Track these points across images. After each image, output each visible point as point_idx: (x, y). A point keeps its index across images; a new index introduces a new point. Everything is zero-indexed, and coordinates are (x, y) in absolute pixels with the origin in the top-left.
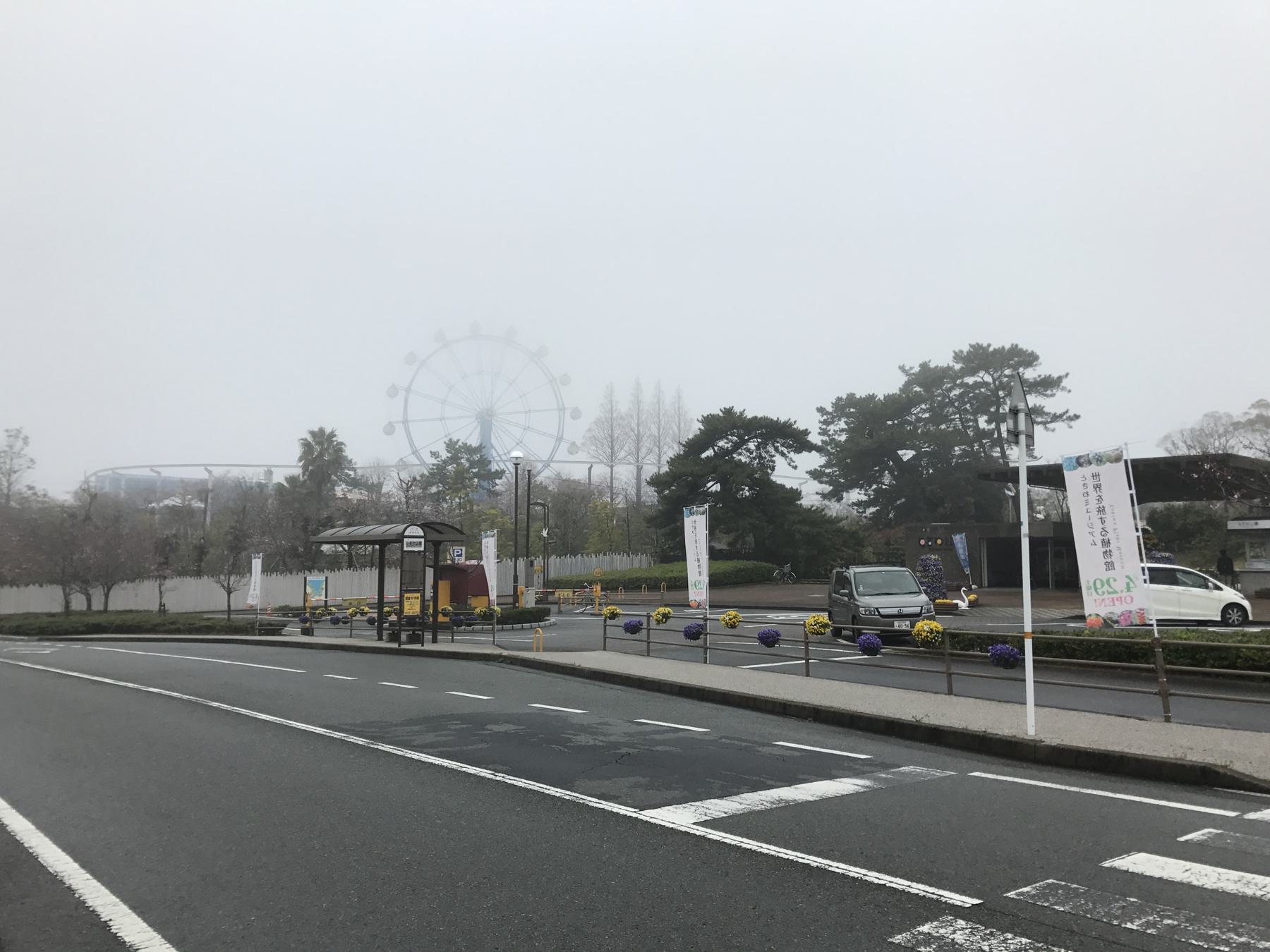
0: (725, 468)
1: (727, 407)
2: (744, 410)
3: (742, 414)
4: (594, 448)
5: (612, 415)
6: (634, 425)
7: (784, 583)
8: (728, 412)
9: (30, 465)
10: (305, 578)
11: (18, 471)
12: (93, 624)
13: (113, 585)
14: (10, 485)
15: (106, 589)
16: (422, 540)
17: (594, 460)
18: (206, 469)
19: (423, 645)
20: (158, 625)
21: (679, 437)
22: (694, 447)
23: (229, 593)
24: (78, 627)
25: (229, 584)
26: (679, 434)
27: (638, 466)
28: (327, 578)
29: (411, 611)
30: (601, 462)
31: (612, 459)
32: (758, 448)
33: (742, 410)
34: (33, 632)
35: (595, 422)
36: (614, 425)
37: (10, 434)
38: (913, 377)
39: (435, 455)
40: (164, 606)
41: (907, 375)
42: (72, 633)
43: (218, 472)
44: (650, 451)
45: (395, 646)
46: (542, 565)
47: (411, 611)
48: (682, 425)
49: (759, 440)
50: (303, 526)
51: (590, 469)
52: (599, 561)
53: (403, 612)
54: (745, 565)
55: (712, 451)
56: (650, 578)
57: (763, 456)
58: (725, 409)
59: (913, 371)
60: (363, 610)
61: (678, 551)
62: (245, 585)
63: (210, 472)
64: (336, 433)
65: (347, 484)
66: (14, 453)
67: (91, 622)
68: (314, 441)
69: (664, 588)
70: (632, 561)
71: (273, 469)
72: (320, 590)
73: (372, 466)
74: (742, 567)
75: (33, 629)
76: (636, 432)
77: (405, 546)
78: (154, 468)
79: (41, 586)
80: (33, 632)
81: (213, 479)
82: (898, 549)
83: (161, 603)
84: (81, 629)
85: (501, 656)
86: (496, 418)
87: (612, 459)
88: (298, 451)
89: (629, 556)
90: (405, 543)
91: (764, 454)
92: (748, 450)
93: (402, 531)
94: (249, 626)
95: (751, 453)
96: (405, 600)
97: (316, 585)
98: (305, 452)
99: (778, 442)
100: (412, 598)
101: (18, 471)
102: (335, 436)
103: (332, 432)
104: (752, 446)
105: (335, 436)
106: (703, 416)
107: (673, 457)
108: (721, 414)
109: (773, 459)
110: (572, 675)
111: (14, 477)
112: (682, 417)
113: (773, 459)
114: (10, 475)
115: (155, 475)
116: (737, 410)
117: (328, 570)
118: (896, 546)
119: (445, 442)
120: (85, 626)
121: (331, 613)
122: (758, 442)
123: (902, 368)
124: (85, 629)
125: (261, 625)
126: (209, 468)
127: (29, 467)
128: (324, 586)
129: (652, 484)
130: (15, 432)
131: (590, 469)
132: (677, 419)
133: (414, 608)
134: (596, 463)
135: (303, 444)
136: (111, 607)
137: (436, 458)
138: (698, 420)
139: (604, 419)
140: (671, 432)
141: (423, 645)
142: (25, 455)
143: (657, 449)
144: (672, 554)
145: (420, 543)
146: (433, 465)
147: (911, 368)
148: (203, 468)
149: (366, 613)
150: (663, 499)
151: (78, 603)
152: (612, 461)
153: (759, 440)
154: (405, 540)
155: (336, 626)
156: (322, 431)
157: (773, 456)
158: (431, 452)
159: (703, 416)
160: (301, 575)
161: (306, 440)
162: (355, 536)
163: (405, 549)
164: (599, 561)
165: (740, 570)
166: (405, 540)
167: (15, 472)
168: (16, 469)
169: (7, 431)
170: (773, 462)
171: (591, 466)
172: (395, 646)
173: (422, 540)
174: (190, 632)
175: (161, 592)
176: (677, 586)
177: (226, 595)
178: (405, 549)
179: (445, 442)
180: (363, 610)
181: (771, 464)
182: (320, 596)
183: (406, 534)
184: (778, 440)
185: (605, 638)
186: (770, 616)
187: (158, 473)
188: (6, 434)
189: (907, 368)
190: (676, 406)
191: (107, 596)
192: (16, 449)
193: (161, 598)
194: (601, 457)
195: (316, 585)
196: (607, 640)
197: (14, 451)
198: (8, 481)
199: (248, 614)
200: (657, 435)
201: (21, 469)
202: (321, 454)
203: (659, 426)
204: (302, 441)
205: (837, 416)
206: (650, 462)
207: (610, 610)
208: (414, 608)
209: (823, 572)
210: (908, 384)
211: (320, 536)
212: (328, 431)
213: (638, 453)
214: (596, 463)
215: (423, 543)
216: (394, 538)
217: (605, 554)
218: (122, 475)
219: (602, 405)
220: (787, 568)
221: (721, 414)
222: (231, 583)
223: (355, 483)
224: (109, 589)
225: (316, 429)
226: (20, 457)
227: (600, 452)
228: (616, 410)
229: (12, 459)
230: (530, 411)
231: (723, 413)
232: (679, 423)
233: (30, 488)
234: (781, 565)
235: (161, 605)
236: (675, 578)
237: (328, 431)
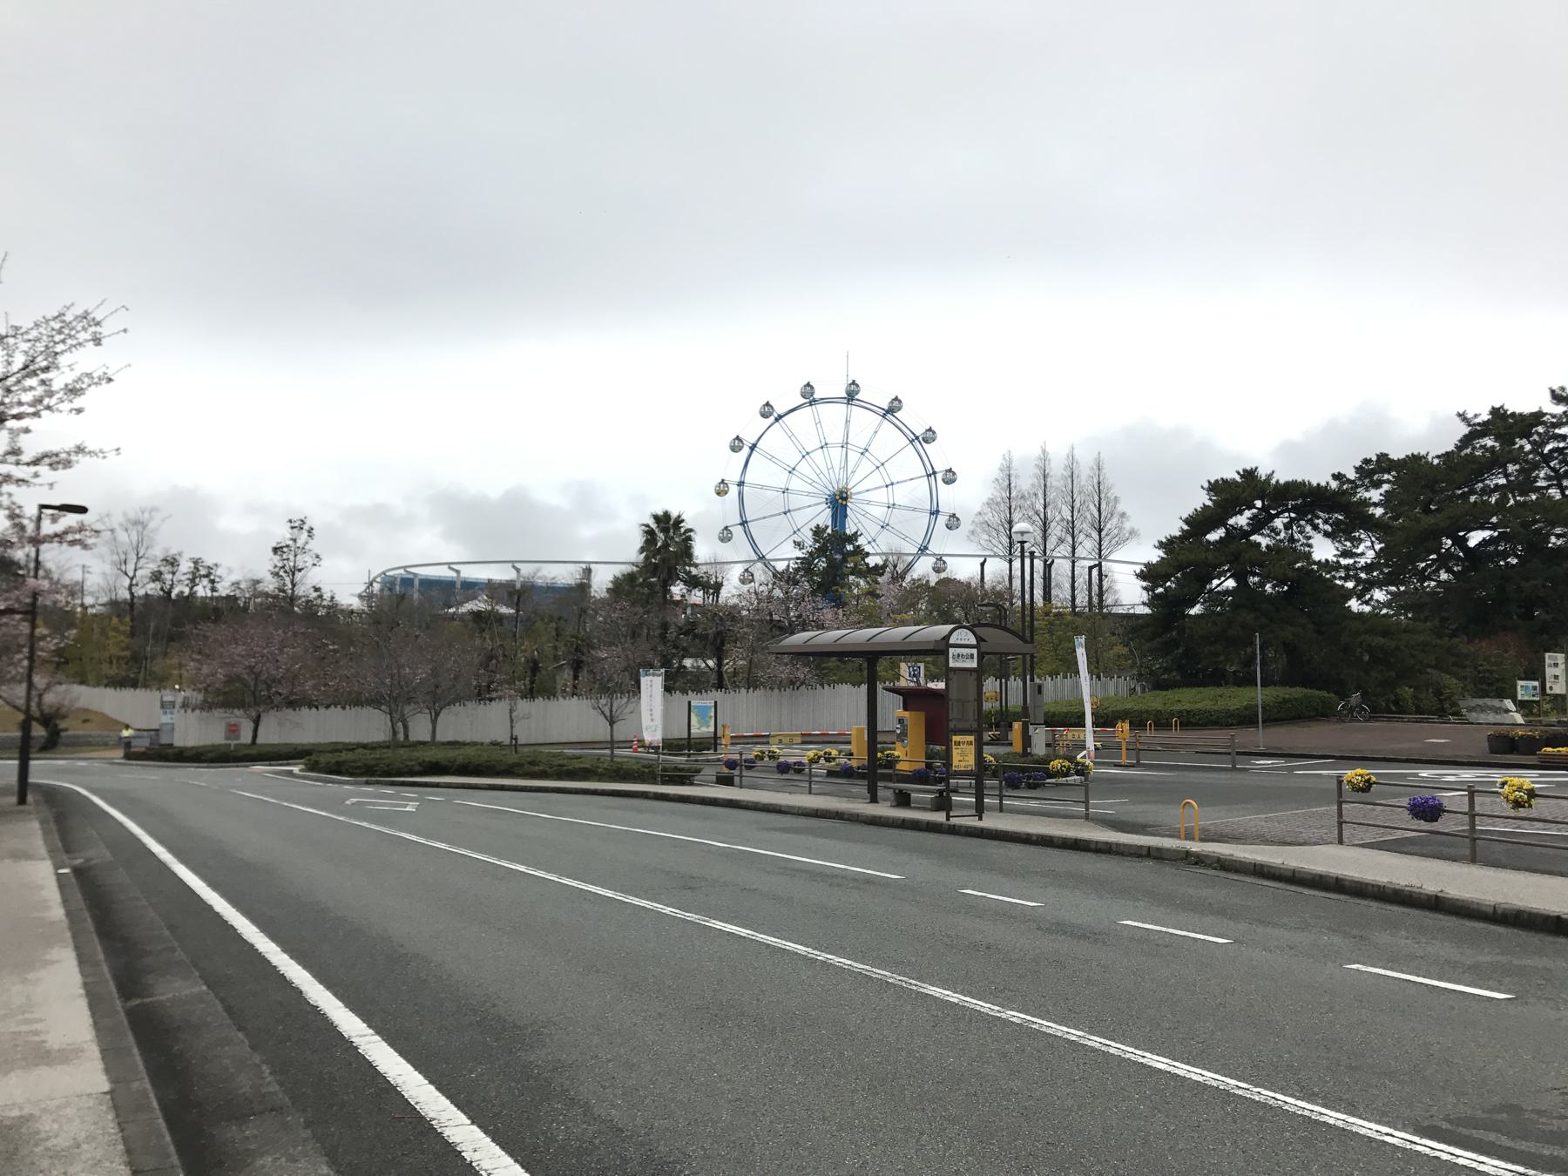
0: (1237, 553)
1: (1248, 468)
2: (1273, 472)
3: (1270, 476)
4: (986, 537)
5: (1010, 494)
6: (1040, 507)
7: (1354, 720)
8: (1249, 475)
9: (315, 562)
10: (689, 703)
11: (302, 569)
12: (430, 762)
13: (441, 709)
14: (294, 585)
15: (433, 714)
16: (975, 651)
17: (988, 553)
18: (514, 567)
19: (980, 819)
20: (516, 765)
21: (1100, 522)
22: (1199, 523)
23: (612, 723)
24: (413, 766)
25: (611, 711)
26: (1100, 518)
27: (1045, 561)
28: (716, 703)
29: (963, 764)
30: (995, 556)
31: (1010, 551)
32: (1287, 526)
33: (1269, 472)
34: (358, 771)
35: (988, 504)
36: (1013, 507)
37: (293, 525)
38: (1479, 428)
39: (799, 545)
40: (516, 739)
41: (1469, 425)
42: (400, 774)
43: (526, 570)
44: (1061, 540)
45: (939, 817)
46: (998, 691)
47: (963, 764)
48: (1103, 506)
49: (1293, 515)
50: (660, 635)
51: (982, 565)
52: (1056, 684)
53: (952, 765)
54: (1291, 694)
55: (1224, 530)
56: (1147, 712)
57: (1296, 537)
58: (1245, 471)
59: (1478, 420)
60: (830, 754)
61: (1174, 674)
62: (631, 712)
63: (518, 570)
64: (683, 517)
65: (686, 583)
66: (299, 548)
67: (427, 759)
68: (658, 527)
69: (1176, 726)
70: (1105, 688)
71: (592, 566)
72: (708, 719)
73: (708, 561)
74: (1287, 696)
75: (358, 767)
76: (1042, 516)
77: (951, 660)
78: (452, 566)
79: (344, 708)
80: (358, 771)
81: (522, 579)
82: (1491, 672)
83: (512, 735)
84: (417, 768)
85: (1188, 854)
86: (851, 500)
87: (1010, 551)
88: (638, 540)
89: (1099, 680)
90: (951, 655)
91: (1297, 536)
92: (1273, 530)
93: (946, 633)
94: (647, 770)
95: (1278, 534)
96: (954, 747)
97: (703, 711)
98: (647, 541)
99: (1318, 517)
100: (964, 743)
101: (302, 569)
102: (683, 521)
103: (679, 516)
104: (1279, 523)
105: (683, 521)
106: (1209, 482)
107: (1164, 540)
108: (1238, 478)
109: (1310, 541)
110: (978, 837)
111: (298, 576)
112: (1102, 496)
113: (1310, 541)
114: (293, 574)
115: (454, 574)
116: (1263, 473)
117: (693, 691)
118: (1488, 668)
119: (811, 530)
120: (420, 764)
121: (773, 757)
122: (1290, 517)
123: (1462, 416)
124: (421, 769)
125: (664, 770)
126: (517, 565)
127: (315, 565)
128: (713, 714)
129: (1140, 576)
130: (300, 522)
131: (982, 565)
132: (1096, 498)
133: (966, 758)
134: (990, 556)
135: (646, 532)
136: (440, 737)
137: (800, 549)
138: (1202, 487)
139: (999, 500)
140: (1089, 516)
141: (980, 819)
142: (310, 550)
143: (1069, 539)
144: (1166, 676)
145: (972, 656)
146: (798, 558)
147: (1476, 416)
148: (510, 565)
149: (834, 759)
150: (1153, 601)
151: (420, 729)
152: (1010, 554)
153: (1293, 515)
154: (951, 651)
155: (785, 776)
156: (667, 515)
157: (1309, 538)
158: (795, 542)
159: (1209, 482)
160: (685, 699)
161: (648, 526)
162: (843, 645)
163: (952, 664)
164: (1056, 684)
165: (1285, 701)
166: (951, 651)
167: (300, 570)
168: (300, 567)
169: (290, 521)
170: (1310, 546)
171: (985, 561)
172: (939, 817)
173: (975, 651)
174: (559, 777)
175: (512, 721)
176: (1191, 722)
177: (609, 727)
178: (952, 664)
179: (811, 530)
180: (830, 754)
181: (1307, 549)
182: (708, 726)
183: (952, 641)
184: (1321, 514)
185: (1340, 824)
186: (1424, 773)
187: (458, 572)
188: (289, 524)
189: (1469, 416)
190: (1095, 481)
191: (434, 722)
192: (300, 543)
193: (512, 727)
194: (995, 549)
195: (703, 711)
196: (1344, 825)
197: (298, 545)
198: (292, 581)
199: (593, 749)
200: (1070, 519)
201: (306, 567)
202: (666, 545)
203: (1073, 507)
204: (643, 528)
205: (1361, 486)
206: (1060, 555)
207: (1362, 776)
208: (966, 758)
209: (1384, 704)
210: (1466, 441)
211: (782, 643)
212: (674, 514)
213: (1045, 544)
214: (990, 556)
215: (975, 656)
216: (932, 648)
217: (1065, 677)
218: (415, 575)
219: (997, 480)
220: (1355, 698)
221: (1238, 478)
222: (614, 709)
223: (693, 582)
224: (437, 715)
225: (660, 513)
226: (305, 553)
227: (993, 541)
228: (1015, 487)
229: (296, 556)
230: (789, 511)
231: (1242, 476)
232: (1100, 505)
233: (317, 589)
234: (1344, 695)
235: (512, 738)
236: (1188, 712)
237: (674, 514)
